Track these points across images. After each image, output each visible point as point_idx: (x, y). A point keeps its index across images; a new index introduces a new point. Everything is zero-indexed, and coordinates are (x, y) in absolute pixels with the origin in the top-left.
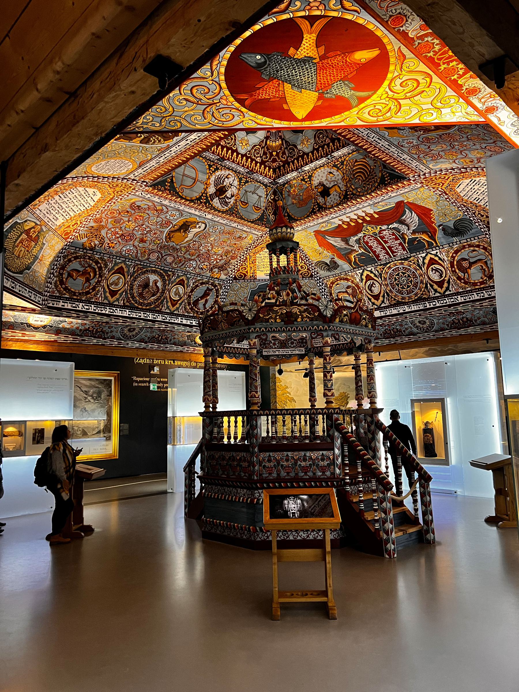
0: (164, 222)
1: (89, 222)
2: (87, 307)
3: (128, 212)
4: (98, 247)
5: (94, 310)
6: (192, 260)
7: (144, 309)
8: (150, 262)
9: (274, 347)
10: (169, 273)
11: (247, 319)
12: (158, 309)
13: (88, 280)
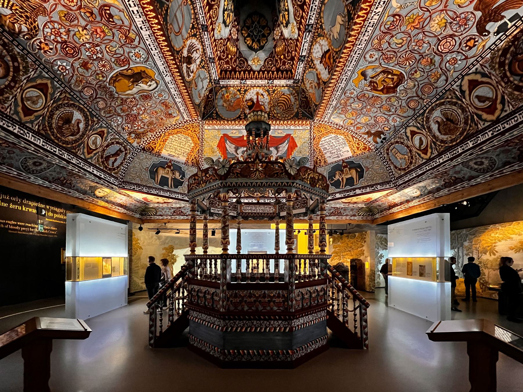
0: (123, 58)
3: (92, 13)
4: (24, 36)
7: (61, 146)
8: (82, 97)
10: (95, 119)
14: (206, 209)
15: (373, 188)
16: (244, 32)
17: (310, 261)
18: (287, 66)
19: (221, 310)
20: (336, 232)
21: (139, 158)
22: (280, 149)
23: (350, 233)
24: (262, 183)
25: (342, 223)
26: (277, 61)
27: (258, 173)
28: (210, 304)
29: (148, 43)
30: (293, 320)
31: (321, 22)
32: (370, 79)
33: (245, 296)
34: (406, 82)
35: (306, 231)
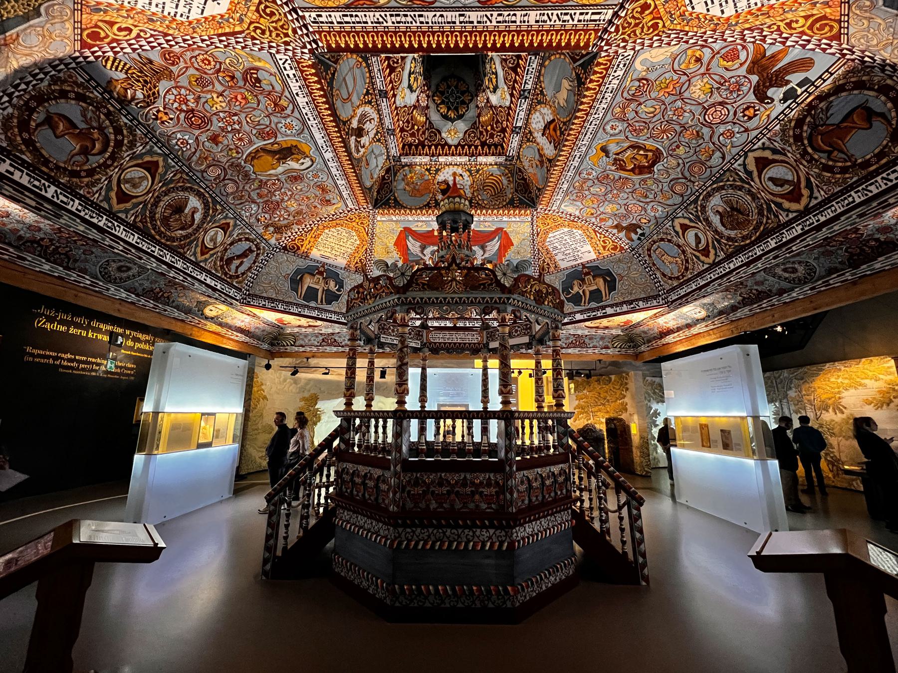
0: (268, 129)
1: (153, 48)
2: (65, 200)
3: (233, 78)
4: (137, 104)
5: (77, 209)
6: (255, 203)
7: (162, 243)
10: (218, 207)
11: (504, 285)
12: (182, 251)
13: (85, 152)
14: (373, 336)
20: (578, 374)
26: (481, 133)
28: (372, 498)
29: (304, 111)
35: (531, 372)
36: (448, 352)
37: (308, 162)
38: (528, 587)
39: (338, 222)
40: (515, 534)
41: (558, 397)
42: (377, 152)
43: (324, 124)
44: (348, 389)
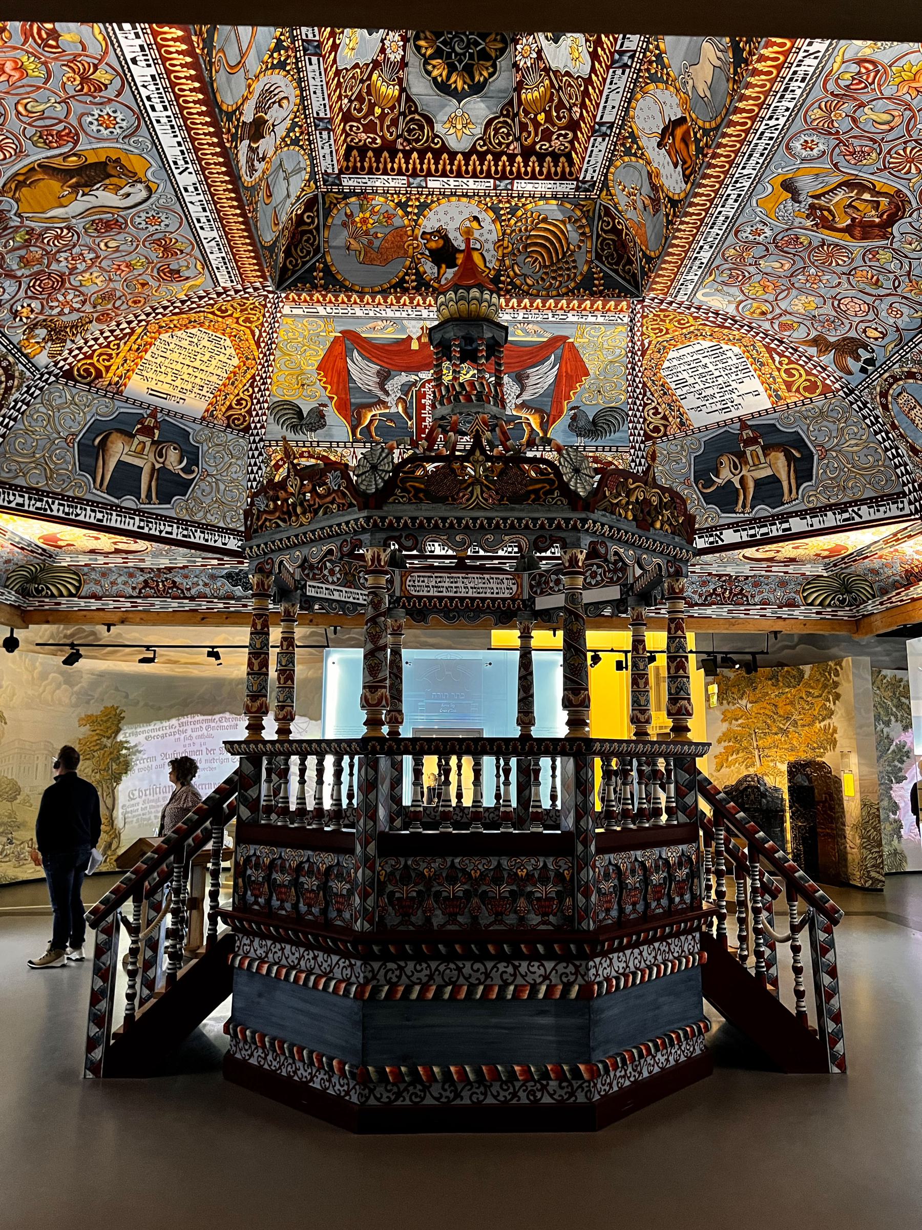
0: (60, 127)
5: (139, 527)
9: (330, 580)
11: (576, 493)
14: (291, 583)
15: (846, 515)
16: (422, 43)
17: (640, 765)
18: (556, 143)
19: (358, 926)
20: (728, 662)
21: (49, 405)
22: (531, 381)
23: (781, 665)
24: (490, 520)
25: (751, 630)
26: (523, 127)
27: (478, 490)
28: (315, 910)
29: (144, 93)
30: (592, 959)
31: (657, 47)
32: (810, 200)
33: (437, 876)
34: (915, 215)
35: (621, 657)
36: (447, 618)
37: (139, 192)
38: (616, 1067)
39: (193, 316)
40: (593, 971)
41: (679, 712)
42: (289, 166)
43: (185, 119)
44: (254, 697)
